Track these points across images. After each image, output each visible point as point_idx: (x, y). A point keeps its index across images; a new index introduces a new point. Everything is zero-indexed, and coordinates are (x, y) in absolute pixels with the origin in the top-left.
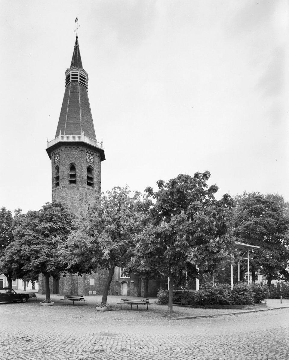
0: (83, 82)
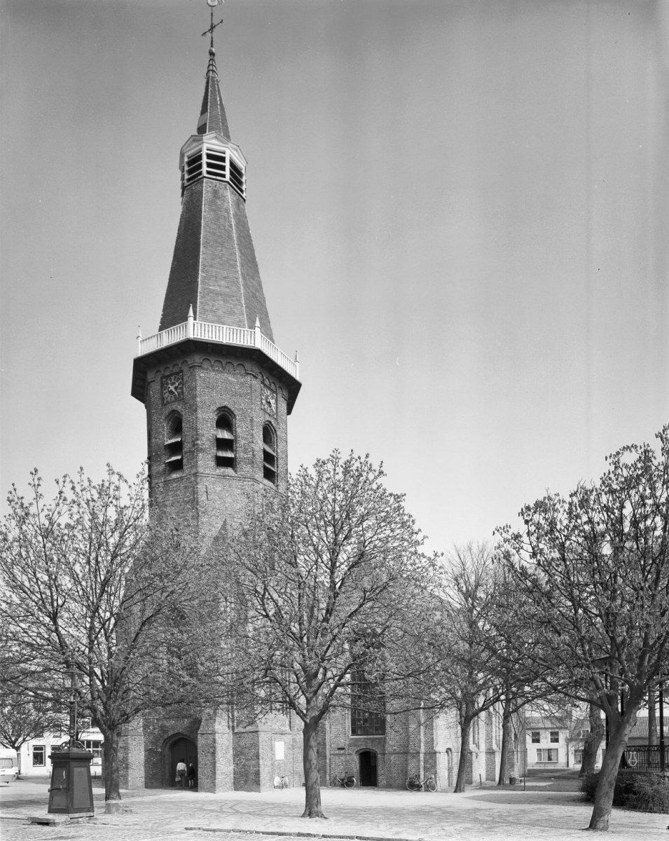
0: (239, 192)
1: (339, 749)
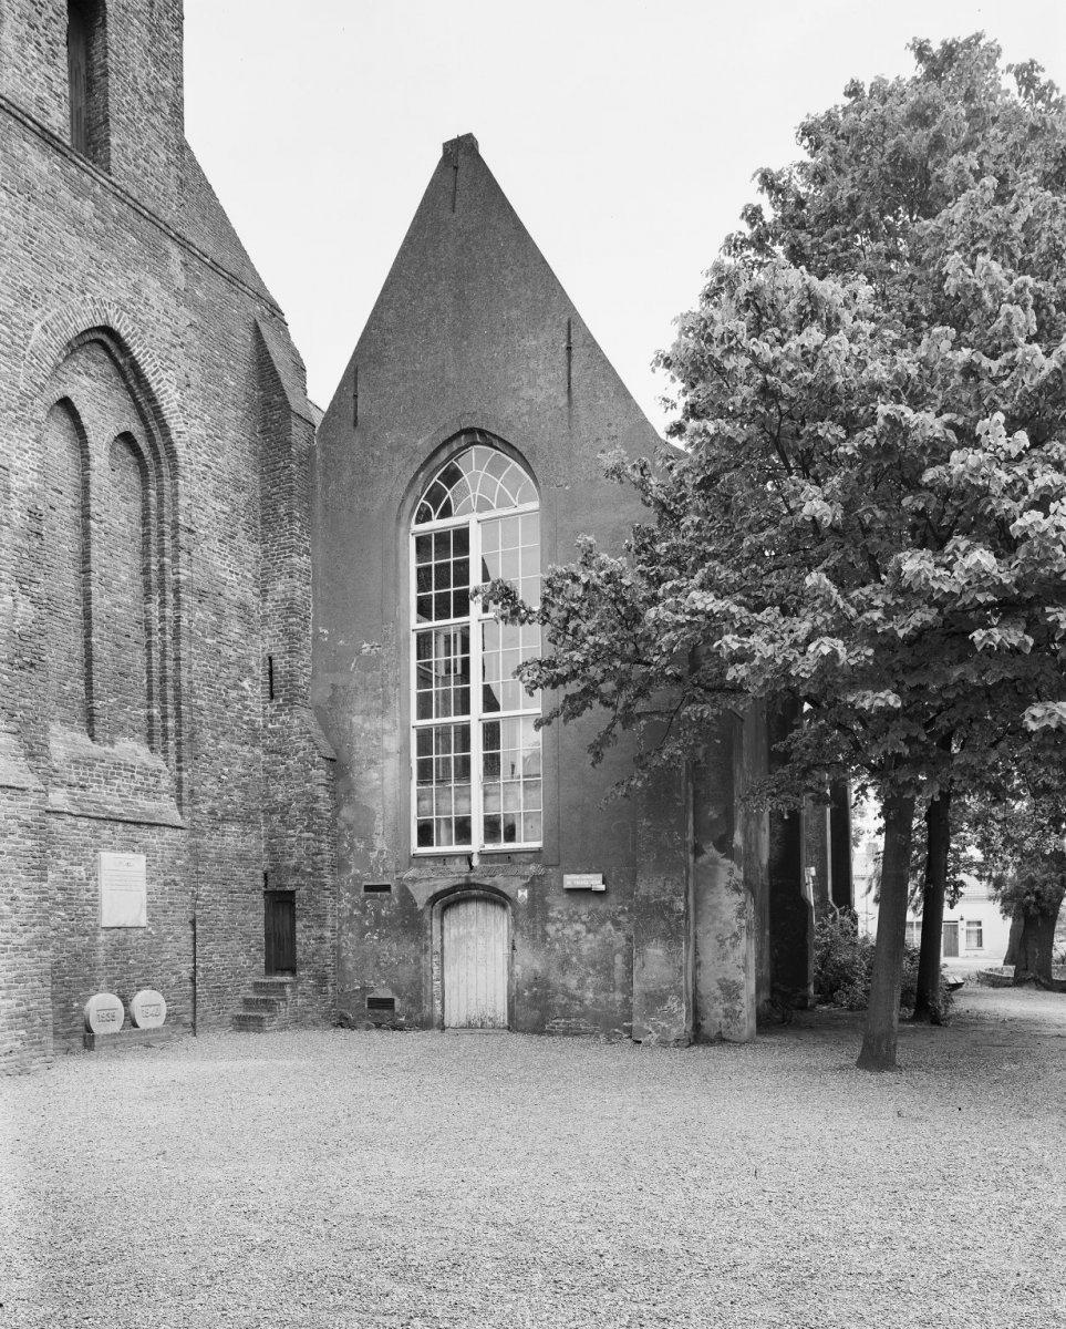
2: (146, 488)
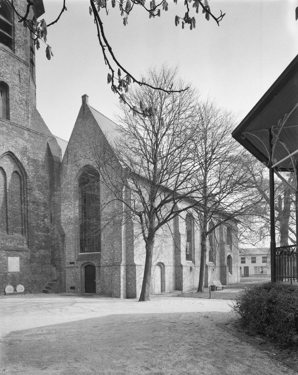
1: (71, 263)
2: (21, 181)
